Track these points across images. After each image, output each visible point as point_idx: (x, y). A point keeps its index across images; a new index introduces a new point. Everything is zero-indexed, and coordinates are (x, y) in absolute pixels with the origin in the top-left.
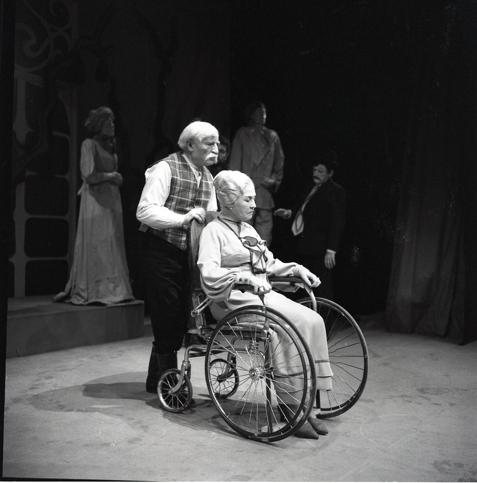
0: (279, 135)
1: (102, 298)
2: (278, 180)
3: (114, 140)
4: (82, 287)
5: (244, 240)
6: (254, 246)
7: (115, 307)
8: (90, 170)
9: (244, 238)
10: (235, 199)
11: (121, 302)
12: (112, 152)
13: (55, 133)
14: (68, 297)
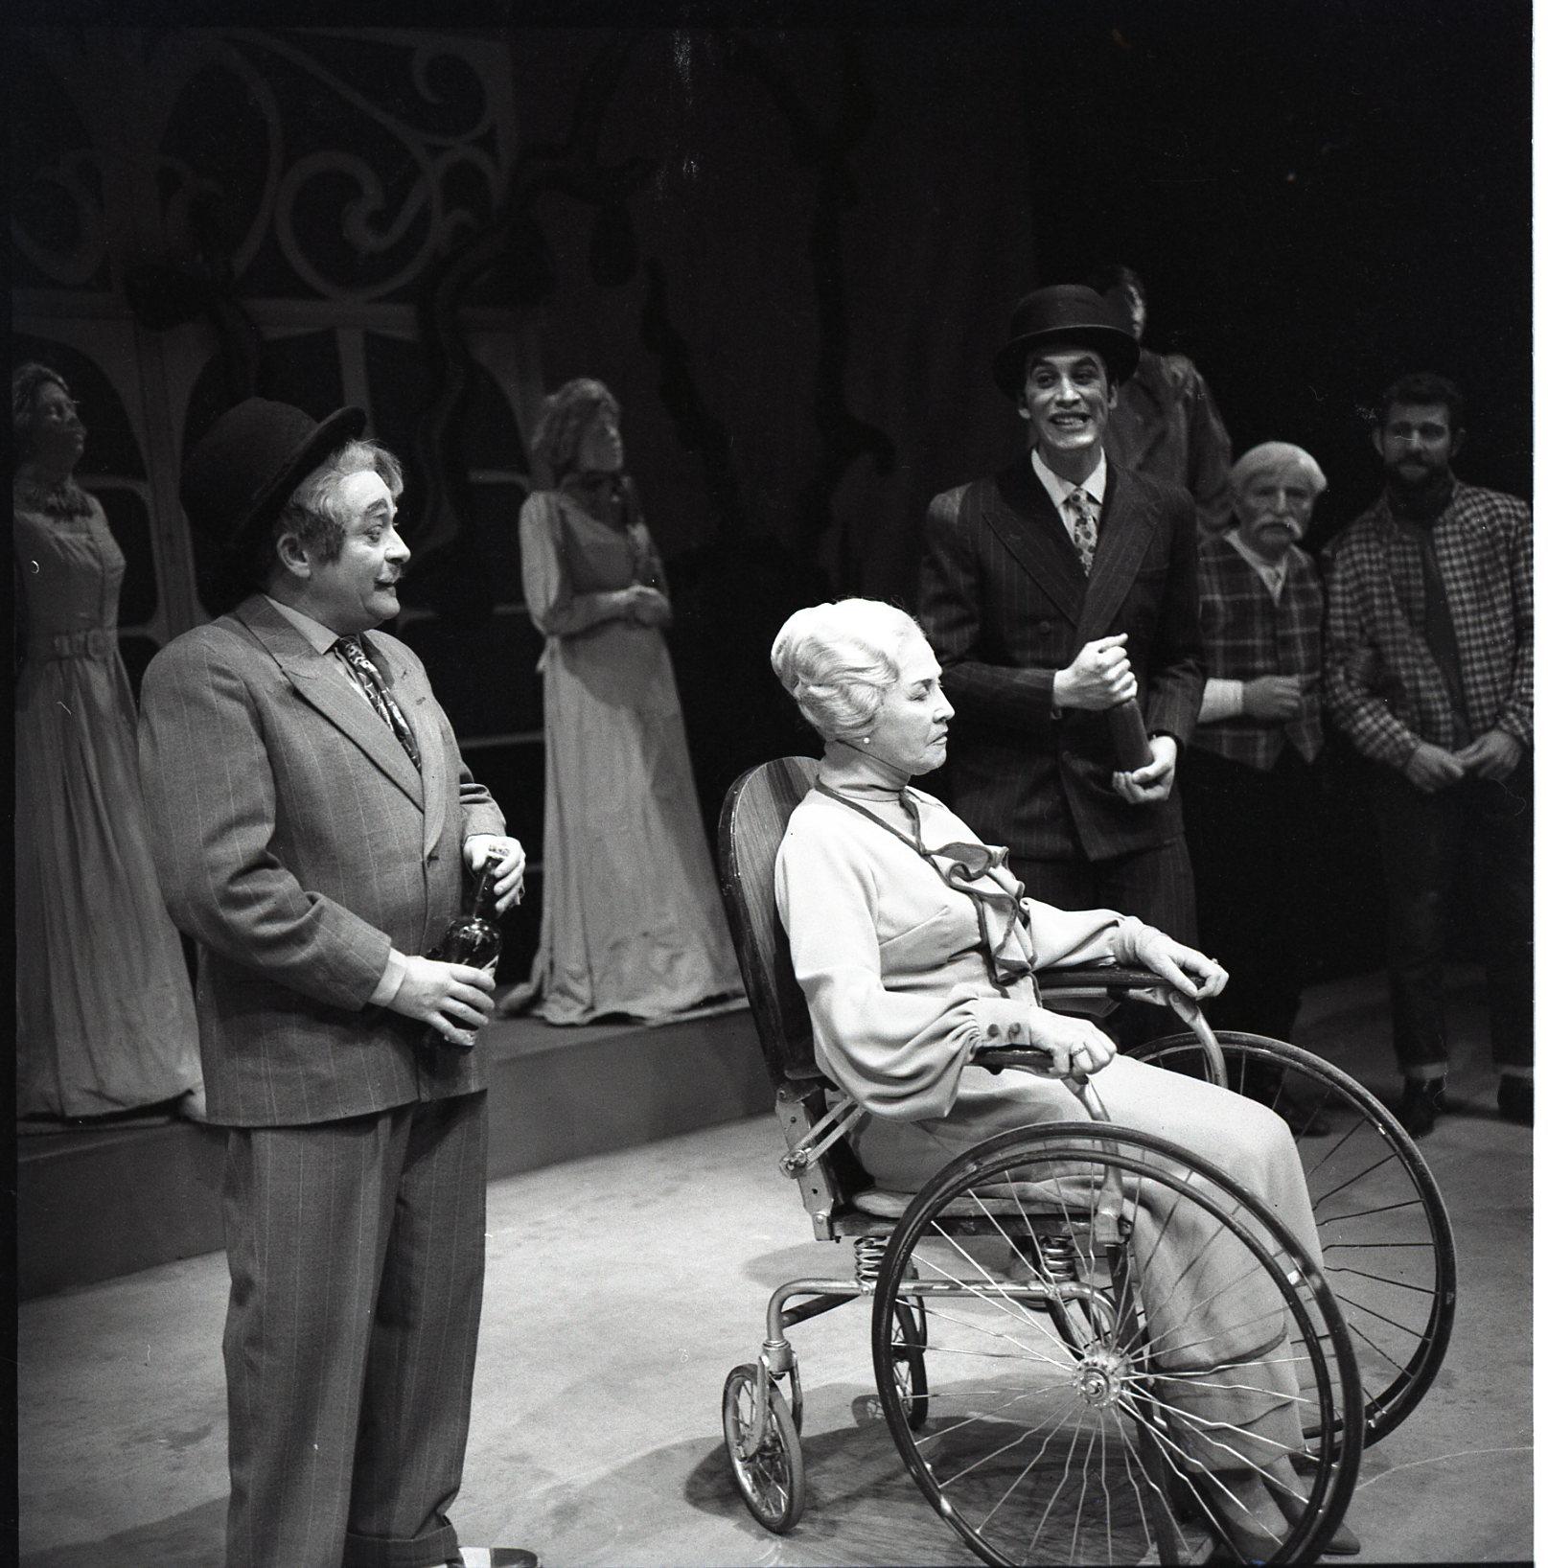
1: (631, 997)
3: (626, 481)
4: (576, 967)
5: (946, 863)
6: (980, 875)
7: (677, 1024)
8: (547, 596)
9: (941, 852)
11: (694, 1007)
12: (621, 522)
13: (479, 477)
14: (537, 999)
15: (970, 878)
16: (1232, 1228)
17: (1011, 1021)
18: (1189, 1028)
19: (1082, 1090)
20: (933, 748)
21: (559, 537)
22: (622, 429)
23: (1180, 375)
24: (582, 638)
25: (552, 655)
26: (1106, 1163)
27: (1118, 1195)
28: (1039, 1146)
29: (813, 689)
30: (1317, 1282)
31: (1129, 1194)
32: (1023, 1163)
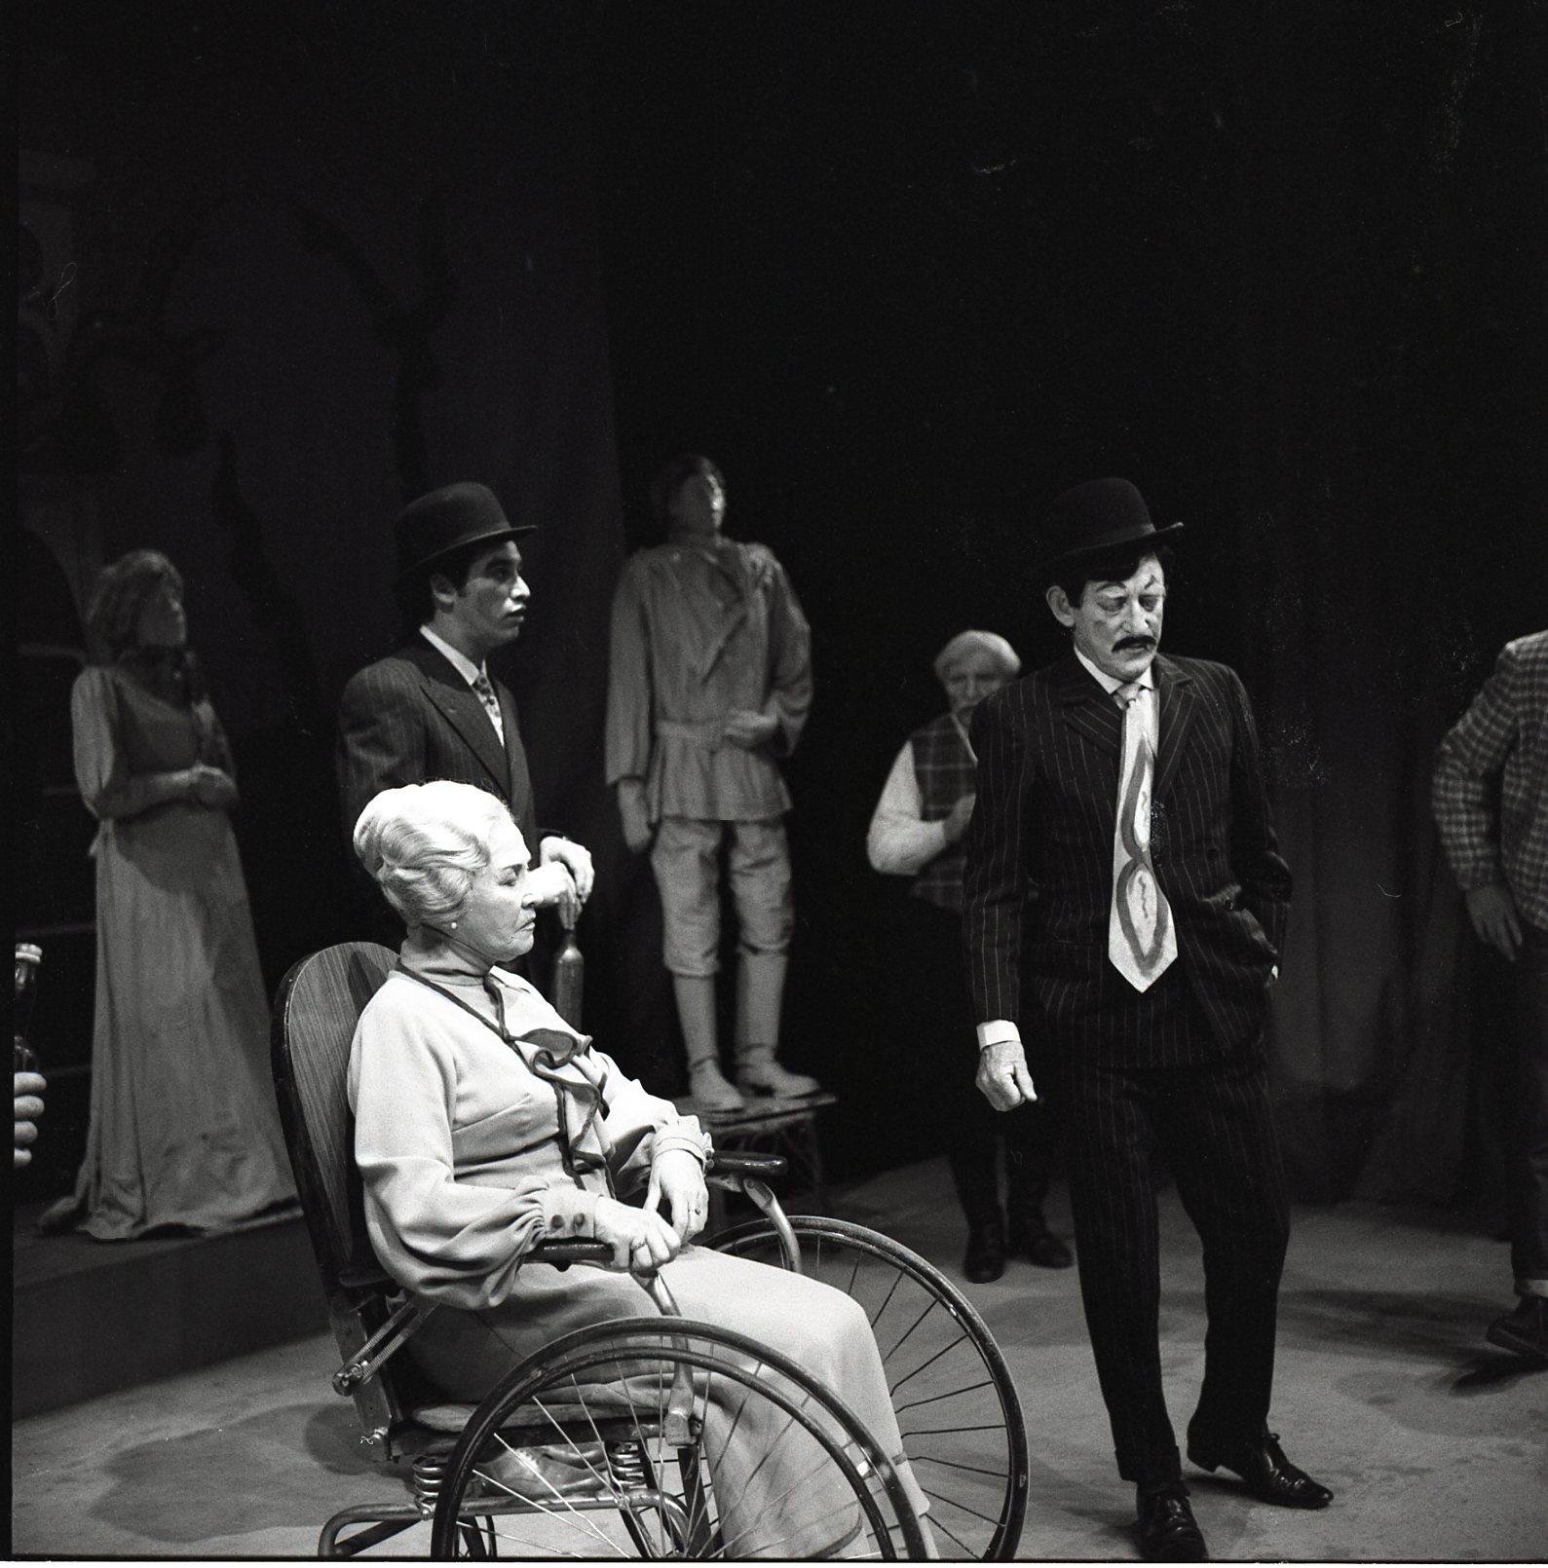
0: (778, 555)
2: (794, 713)
3: (189, 656)
5: (530, 1050)
6: (563, 1063)
7: (238, 1235)
10: (463, 887)
11: (258, 1214)
12: (185, 699)
14: (82, 1213)
15: (553, 1066)
16: (801, 1420)
17: (577, 1210)
18: (761, 1213)
19: (651, 1284)
20: (523, 933)
21: (115, 715)
22: (184, 604)
23: (760, 563)
24: (141, 818)
25: (106, 838)
26: (676, 1360)
27: (688, 1391)
28: (607, 1345)
29: (400, 872)
30: (886, 1471)
31: (699, 1390)
32: (590, 1365)
